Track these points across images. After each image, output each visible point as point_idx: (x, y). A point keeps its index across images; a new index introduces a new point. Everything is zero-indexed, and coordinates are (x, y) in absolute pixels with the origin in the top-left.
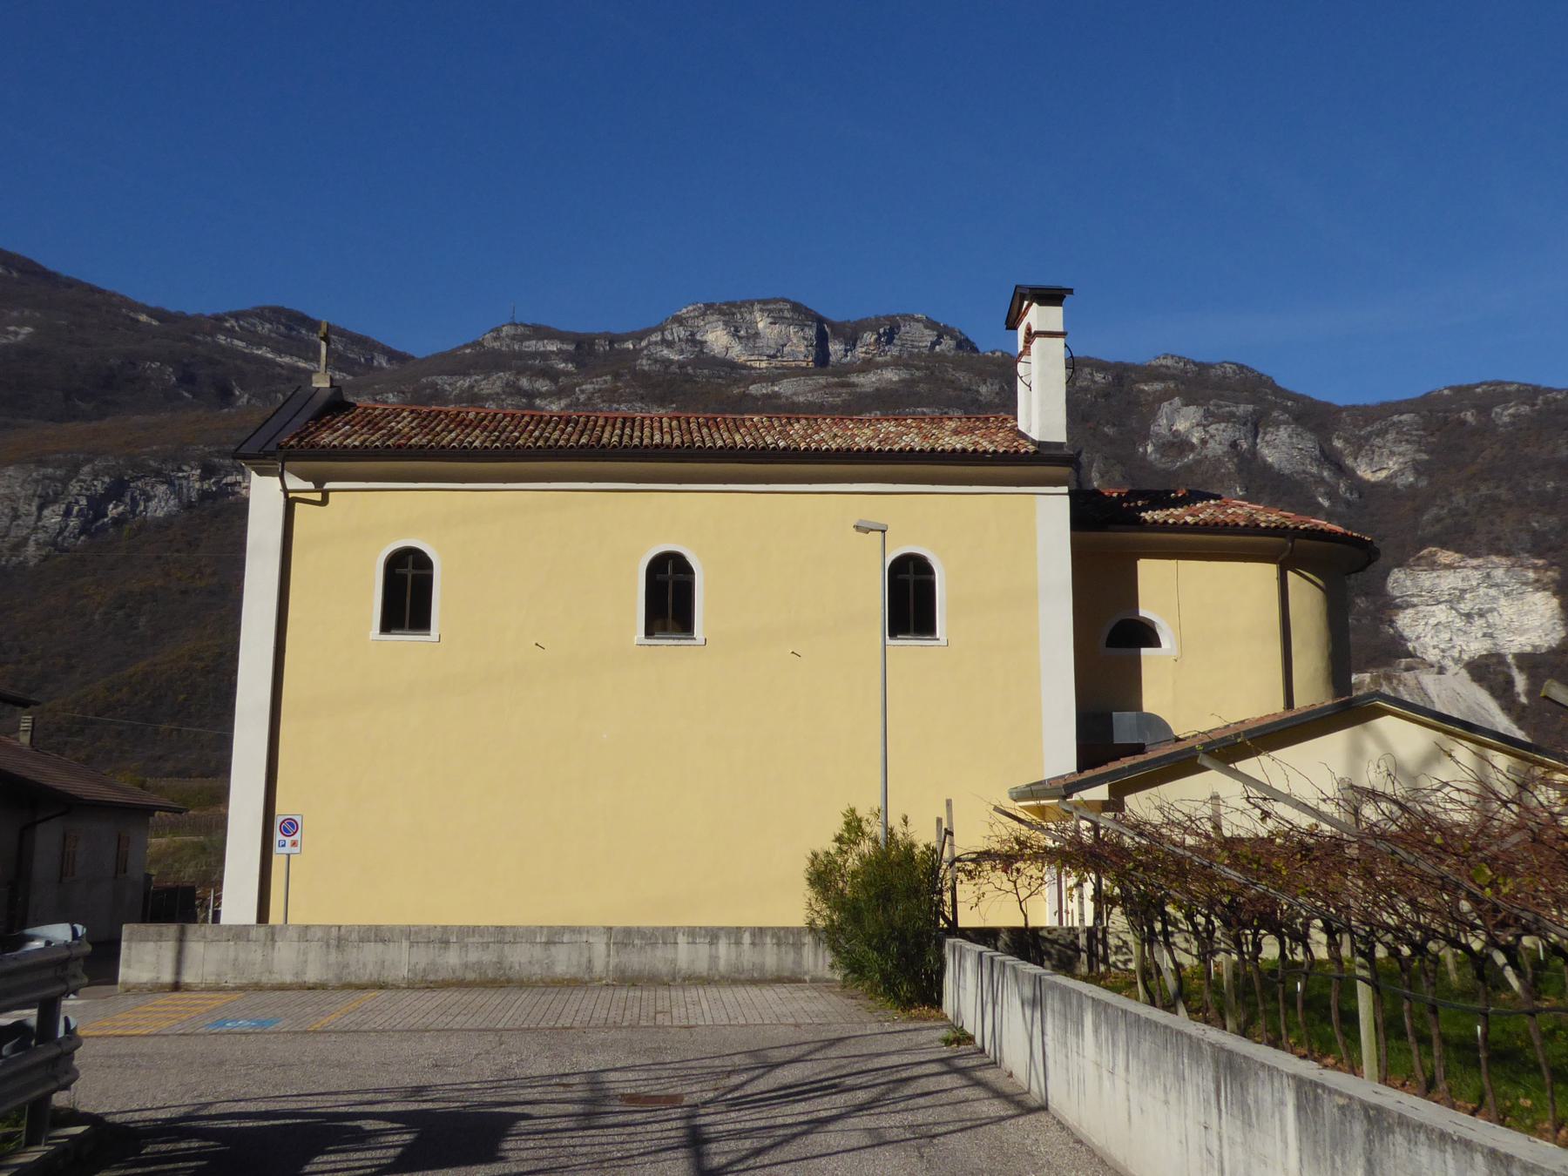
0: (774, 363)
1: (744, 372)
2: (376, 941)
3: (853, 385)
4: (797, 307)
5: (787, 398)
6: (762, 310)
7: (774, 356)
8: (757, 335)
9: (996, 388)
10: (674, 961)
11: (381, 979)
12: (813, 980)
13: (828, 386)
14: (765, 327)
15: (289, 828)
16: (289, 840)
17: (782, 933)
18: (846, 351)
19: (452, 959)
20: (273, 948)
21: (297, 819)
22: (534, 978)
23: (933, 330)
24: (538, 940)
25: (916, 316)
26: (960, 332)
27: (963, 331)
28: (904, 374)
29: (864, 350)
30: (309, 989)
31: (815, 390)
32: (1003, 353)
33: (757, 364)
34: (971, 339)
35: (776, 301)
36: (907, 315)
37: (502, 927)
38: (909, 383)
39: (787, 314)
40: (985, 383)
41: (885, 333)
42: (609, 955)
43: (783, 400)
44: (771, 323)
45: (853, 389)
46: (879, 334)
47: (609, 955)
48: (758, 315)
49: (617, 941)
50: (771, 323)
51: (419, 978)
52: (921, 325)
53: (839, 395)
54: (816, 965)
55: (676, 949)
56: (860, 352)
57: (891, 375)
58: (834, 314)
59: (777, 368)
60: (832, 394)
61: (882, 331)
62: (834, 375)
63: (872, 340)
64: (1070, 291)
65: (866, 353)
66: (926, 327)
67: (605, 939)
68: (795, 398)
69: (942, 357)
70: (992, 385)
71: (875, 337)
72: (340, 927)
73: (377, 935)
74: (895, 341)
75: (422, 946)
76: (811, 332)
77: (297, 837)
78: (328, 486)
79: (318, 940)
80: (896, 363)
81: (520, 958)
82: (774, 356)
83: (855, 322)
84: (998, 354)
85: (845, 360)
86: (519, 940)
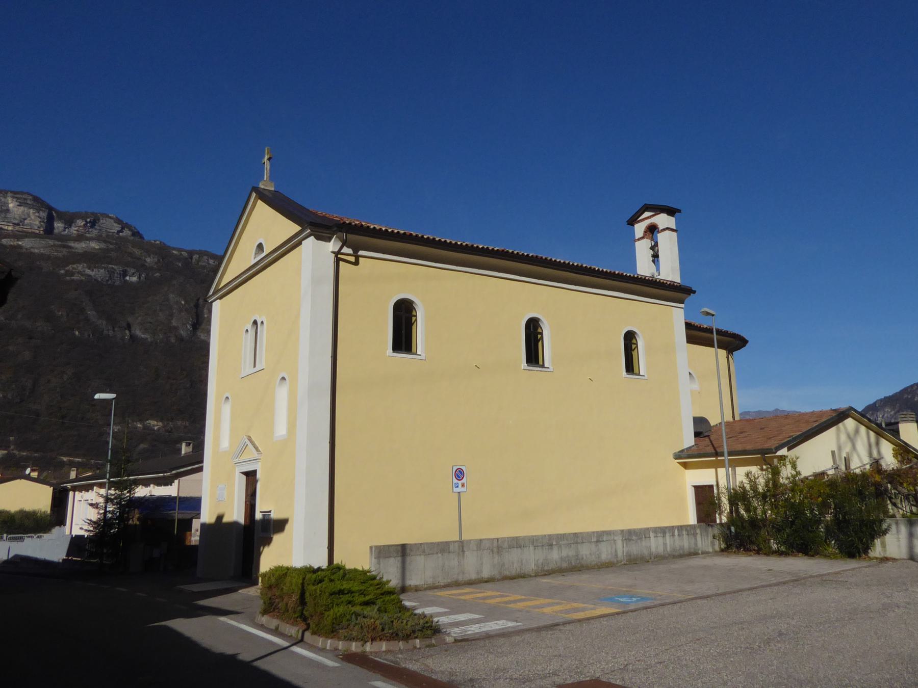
0: (17, 228)
1: (3, 231)
2: (517, 547)
3: (71, 247)
4: (36, 199)
5: (27, 249)
6: (13, 197)
7: (18, 224)
8: (8, 210)
9: (156, 260)
10: (649, 548)
11: (522, 572)
12: (703, 553)
13: (54, 246)
14: (14, 207)
15: (460, 475)
16: (460, 482)
17: (689, 528)
18: (65, 228)
19: (555, 555)
20: (463, 556)
21: (463, 468)
22: (593, 563)
23: (119, 224)
24: (593, 540)
25: (110, 215)
26: (135, 228)
27: (137, 228)
28: (103, 246)
29: (76, 229)
30: (486, 582)
31: (46, 247)
32: (161, 242)
33: (6, 227)
34: (141, 232)
35: (22, 193)
36: (105, 214)
37: (576, 533)
38: (107, 250)
39: (29, 202)
40: (149, 257)
41: (90, 222)
42: (623, 547)
43: (24, 250)
44: (18, 205)
45: (70, 250)
46: (86, 221)
47: (623, 547)
48: (10, 200)
49: (626, 538)
50: (18, 205)
51: (540, 569)
52: (112, 221)
53: (61, 252)
54: (702, 545)
55: (650, 539)
56: (73, 230)
57: (95, 245)
58: (61, 204)
59: (18, 231)
60: (57, 251)
61: (88, 220)
62: (58, 240)
63: (82, 224)
64: (679, 211)
65: (77, 231)
66: (115, 222)
67: (621, 538)
68: (32, 250)
69: (124, 239)
70: (153, 258)
71: (84, 223)
72: (498, 539)
73: (517, 543)
74: (96, 227)
75: (540, 548)
76: (44, 214)
77: (464, 481)
78: (361, 253)
79: (487, 550)
80: (98, 239)
81: (586, 552)
82: (18, 224)
83: (73, 213)
84: (158, 242)
85: (63, 233)
86: (584, 541)
